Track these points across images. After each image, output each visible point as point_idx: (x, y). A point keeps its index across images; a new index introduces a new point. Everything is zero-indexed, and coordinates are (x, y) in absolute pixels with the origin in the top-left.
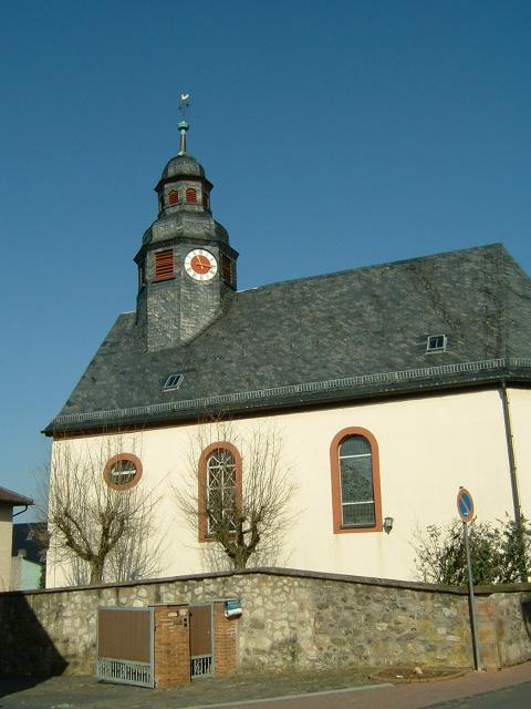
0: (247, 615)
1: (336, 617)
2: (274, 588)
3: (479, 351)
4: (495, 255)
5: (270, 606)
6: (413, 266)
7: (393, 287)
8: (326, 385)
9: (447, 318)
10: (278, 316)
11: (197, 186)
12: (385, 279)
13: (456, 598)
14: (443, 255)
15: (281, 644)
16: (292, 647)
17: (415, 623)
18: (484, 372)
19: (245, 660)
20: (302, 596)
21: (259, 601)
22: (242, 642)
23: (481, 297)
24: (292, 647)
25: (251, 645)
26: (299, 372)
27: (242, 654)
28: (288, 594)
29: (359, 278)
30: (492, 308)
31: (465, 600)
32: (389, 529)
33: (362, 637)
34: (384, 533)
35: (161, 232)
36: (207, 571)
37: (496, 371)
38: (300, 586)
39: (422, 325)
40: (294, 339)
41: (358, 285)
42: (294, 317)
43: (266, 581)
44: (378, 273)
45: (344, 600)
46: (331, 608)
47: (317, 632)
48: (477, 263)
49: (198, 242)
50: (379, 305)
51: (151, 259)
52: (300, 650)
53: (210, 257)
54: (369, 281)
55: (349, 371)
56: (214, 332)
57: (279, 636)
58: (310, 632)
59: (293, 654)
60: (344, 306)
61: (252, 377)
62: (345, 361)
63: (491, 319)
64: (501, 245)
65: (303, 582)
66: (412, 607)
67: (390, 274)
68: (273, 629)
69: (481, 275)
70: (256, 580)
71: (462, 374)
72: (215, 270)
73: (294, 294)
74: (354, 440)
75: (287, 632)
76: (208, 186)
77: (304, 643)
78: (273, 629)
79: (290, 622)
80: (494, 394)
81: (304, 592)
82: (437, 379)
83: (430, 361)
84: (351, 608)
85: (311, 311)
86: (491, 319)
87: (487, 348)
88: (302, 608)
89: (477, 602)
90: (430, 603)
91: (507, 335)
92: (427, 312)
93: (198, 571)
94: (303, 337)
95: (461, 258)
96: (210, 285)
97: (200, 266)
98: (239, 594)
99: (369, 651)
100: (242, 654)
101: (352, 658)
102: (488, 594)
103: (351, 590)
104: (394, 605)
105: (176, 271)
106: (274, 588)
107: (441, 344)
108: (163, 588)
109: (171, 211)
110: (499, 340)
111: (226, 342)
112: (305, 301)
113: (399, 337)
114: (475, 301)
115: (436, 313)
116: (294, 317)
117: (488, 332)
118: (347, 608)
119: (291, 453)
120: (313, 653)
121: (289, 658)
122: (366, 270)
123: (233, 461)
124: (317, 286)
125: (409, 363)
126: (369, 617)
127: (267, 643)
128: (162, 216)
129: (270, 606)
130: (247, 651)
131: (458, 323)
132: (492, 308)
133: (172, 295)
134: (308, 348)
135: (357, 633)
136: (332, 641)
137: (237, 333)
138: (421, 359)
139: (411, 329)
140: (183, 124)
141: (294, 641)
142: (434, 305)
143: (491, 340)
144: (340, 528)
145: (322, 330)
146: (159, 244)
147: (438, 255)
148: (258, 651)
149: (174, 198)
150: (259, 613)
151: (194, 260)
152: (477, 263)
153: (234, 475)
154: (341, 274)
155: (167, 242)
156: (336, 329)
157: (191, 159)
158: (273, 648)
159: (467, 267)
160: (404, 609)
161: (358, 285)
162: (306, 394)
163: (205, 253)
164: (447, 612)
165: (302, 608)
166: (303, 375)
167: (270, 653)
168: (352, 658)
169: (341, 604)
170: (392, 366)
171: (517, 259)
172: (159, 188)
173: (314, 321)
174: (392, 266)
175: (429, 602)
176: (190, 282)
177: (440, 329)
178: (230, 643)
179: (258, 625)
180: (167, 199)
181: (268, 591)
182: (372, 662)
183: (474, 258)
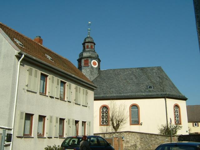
0: (125, 140)
1: (145, 140)
2: (131, 135)
3: (159, 90)
4: (159, 69)
5: (130, 138)
6: (142, 69)
7: (138, 74)
8: (128, 94)
9: (152, 82)
10: (113, 77)
11: (93, 44)
12: (136, 71)
13: (169, 137)
14: (149, 68)
15: (133, 145)
16: (135, 146)
17: (160, 141)
18: (161, 95)
19: (125, 148)
20: (137, 136)
21: (128, 137)
22: (124, 145)
23: (158, 78)
24: (135, 146)
25: (126, 146)
26: (121, 91)
27: (124, 147)
28: (134, 136)
29: (131, 71)
30: (161, 81)
31: (170, 137)
32: (141, 125)
33: (150, 144)
34: (140, 126)
35: (85, 55)
36: (101, 132)
37: (164, 95)
38: (137, 135)
39: (147, 83)
40: (118, 83)
41: (130, 72)
42: (117, 78)
43: (129, 133)
44: (135, 70)
45: (146, 137)
46: (144, 139)
47: (140, 143)
48: (156, 70)
49: (94, 58)
50: (136, 78)
51: (83, 61)
52: (137, 146)
53: (96, 62)
54: (133, 72)
55: (132, 92)
56: (98, 79)
57: (132, 144)
58: (139, 143)
59: (136, 147)
60: (128, 77)
61: (110, 91)
62: (131, 89)
63: (161, 83)
64: (161, 67)
65: (138, 134)
66: (160, 138)
67: (137, 70)
68: (131, 143)
69: (157, 73)
70: (127, 133)
71: (157, 95)
72: (97, 65)
73: (116, 73)
74: (135, 106)
75: (134, 143)
76: (95, 44)
77: (138, 145)
78: (131, 143)
79: (135, 141)
80: (163, 99)
81: (138, 136)
82: (152, 95)
83: (150, 91)
84: (148, 139)
85: (121, 77)
86: (161, 83)
87: (161, 90)
88: (137, 139)
89: (172, 138)
90: (163, 138)
91: (165, 87)
92: (147, 80)
93: (99, 132)
94: (120, 83)
95: (152, 69)
96: (96, 68)
97: (95, 64)
98: (124, 136)
99: (151, 146)
100: (124, 147)
101: (148, 148)
102: (174, 137)
103: (148, 135)
104: (156, 138)
105: (89, 64)
106: (131, 135)
107: (151, 88)
108: (105, 135)
109: (87, 50)
110: (163, 88)
111: (102, 82)
112: (119, 74)
113: (142, 85)
114: (157, 79)
115: (149, 81)
116: (117, 78)
117: (161, 86)
118: (147, 139)
119: (120, 107)
120: (140, 147)
121: (135, 148)
122: (131, 69)
123: (107, 109)
124: (121, 71)
125: (145, 91)
126: (151, 140)
127: (130, 145)
128: (84, 50)
129: (130, 138)
130: (125, 147)
131: (154, 83)
132: (161, 81)
133: (88, 70)
134: (122, 85)
135: (149, 143)
136: (144, 145)
137: (104, 80)
138: (147, 90)
139: (144, 84)
140: (89, 29)
141: (136, 145)
142: (148, 79)
143: (162, 88)
144: (188, 122)
145: (124, 82)
146: (85, 58)
147: (148, 67)
148: (127, 147)
149: (88, 47)
150: (128, 140)
151: (93, 62)
152: (156, 70)
153: (107, 112)
154: (126, 69)
155: (87, 58)
156: (127, 82)
157: (91, 38)
158: (131, 146)
159: (154, 71)
160: (158, 139)
161: (130, 72)
162: (124, 96)
163: (95, 61)
164: (167, 139)
165: (137, 139)
166: (122, 91)
167: (130, 147)
168: (148, 148)
169: (146, 138)
170: (142, 92)
171: (164, 70)
172: (84, 44)
173: (122, 79)
174: (138, 68)
175: (163, 138)
176: (92, 67)
177: (151, 85)
178: (122, 145)
179: (128, 142)
180: (86, 47)
181: (130, 135)
182: (152, 148)
183: (155, 69)
